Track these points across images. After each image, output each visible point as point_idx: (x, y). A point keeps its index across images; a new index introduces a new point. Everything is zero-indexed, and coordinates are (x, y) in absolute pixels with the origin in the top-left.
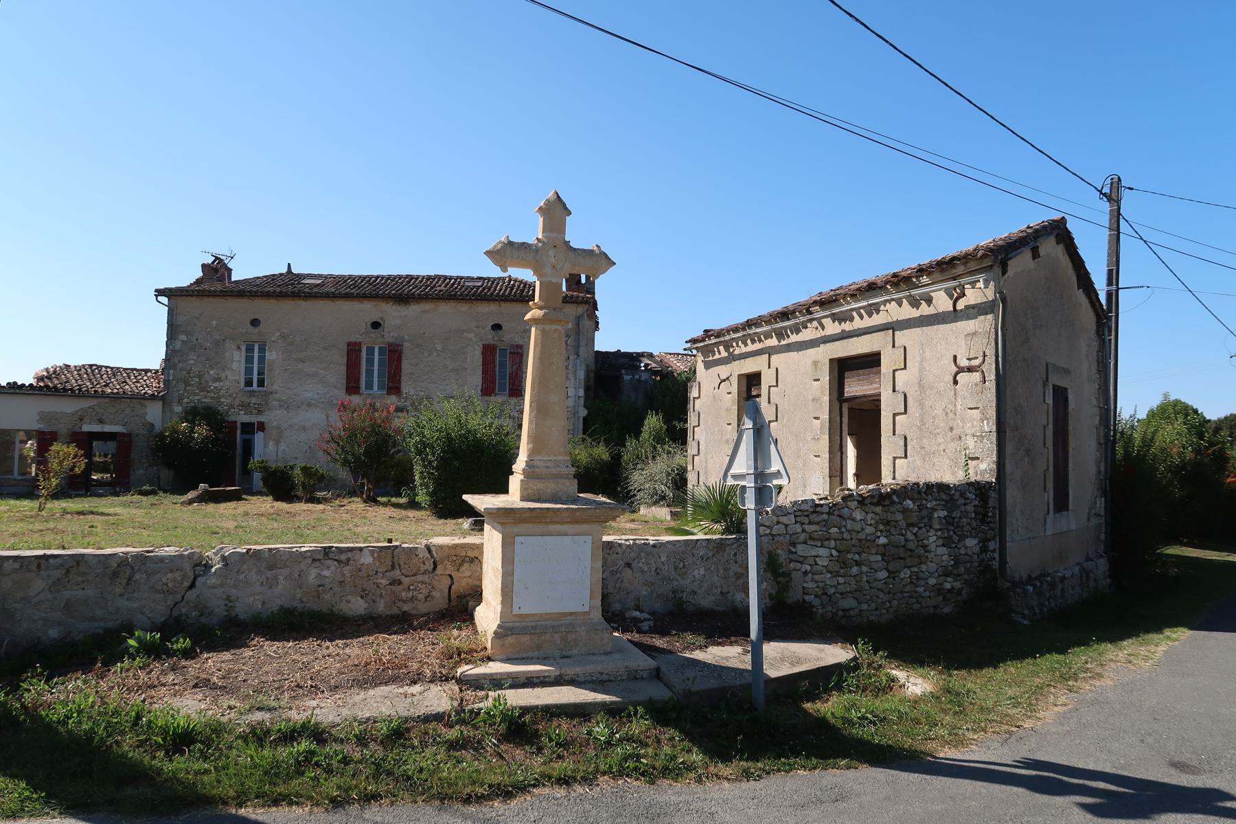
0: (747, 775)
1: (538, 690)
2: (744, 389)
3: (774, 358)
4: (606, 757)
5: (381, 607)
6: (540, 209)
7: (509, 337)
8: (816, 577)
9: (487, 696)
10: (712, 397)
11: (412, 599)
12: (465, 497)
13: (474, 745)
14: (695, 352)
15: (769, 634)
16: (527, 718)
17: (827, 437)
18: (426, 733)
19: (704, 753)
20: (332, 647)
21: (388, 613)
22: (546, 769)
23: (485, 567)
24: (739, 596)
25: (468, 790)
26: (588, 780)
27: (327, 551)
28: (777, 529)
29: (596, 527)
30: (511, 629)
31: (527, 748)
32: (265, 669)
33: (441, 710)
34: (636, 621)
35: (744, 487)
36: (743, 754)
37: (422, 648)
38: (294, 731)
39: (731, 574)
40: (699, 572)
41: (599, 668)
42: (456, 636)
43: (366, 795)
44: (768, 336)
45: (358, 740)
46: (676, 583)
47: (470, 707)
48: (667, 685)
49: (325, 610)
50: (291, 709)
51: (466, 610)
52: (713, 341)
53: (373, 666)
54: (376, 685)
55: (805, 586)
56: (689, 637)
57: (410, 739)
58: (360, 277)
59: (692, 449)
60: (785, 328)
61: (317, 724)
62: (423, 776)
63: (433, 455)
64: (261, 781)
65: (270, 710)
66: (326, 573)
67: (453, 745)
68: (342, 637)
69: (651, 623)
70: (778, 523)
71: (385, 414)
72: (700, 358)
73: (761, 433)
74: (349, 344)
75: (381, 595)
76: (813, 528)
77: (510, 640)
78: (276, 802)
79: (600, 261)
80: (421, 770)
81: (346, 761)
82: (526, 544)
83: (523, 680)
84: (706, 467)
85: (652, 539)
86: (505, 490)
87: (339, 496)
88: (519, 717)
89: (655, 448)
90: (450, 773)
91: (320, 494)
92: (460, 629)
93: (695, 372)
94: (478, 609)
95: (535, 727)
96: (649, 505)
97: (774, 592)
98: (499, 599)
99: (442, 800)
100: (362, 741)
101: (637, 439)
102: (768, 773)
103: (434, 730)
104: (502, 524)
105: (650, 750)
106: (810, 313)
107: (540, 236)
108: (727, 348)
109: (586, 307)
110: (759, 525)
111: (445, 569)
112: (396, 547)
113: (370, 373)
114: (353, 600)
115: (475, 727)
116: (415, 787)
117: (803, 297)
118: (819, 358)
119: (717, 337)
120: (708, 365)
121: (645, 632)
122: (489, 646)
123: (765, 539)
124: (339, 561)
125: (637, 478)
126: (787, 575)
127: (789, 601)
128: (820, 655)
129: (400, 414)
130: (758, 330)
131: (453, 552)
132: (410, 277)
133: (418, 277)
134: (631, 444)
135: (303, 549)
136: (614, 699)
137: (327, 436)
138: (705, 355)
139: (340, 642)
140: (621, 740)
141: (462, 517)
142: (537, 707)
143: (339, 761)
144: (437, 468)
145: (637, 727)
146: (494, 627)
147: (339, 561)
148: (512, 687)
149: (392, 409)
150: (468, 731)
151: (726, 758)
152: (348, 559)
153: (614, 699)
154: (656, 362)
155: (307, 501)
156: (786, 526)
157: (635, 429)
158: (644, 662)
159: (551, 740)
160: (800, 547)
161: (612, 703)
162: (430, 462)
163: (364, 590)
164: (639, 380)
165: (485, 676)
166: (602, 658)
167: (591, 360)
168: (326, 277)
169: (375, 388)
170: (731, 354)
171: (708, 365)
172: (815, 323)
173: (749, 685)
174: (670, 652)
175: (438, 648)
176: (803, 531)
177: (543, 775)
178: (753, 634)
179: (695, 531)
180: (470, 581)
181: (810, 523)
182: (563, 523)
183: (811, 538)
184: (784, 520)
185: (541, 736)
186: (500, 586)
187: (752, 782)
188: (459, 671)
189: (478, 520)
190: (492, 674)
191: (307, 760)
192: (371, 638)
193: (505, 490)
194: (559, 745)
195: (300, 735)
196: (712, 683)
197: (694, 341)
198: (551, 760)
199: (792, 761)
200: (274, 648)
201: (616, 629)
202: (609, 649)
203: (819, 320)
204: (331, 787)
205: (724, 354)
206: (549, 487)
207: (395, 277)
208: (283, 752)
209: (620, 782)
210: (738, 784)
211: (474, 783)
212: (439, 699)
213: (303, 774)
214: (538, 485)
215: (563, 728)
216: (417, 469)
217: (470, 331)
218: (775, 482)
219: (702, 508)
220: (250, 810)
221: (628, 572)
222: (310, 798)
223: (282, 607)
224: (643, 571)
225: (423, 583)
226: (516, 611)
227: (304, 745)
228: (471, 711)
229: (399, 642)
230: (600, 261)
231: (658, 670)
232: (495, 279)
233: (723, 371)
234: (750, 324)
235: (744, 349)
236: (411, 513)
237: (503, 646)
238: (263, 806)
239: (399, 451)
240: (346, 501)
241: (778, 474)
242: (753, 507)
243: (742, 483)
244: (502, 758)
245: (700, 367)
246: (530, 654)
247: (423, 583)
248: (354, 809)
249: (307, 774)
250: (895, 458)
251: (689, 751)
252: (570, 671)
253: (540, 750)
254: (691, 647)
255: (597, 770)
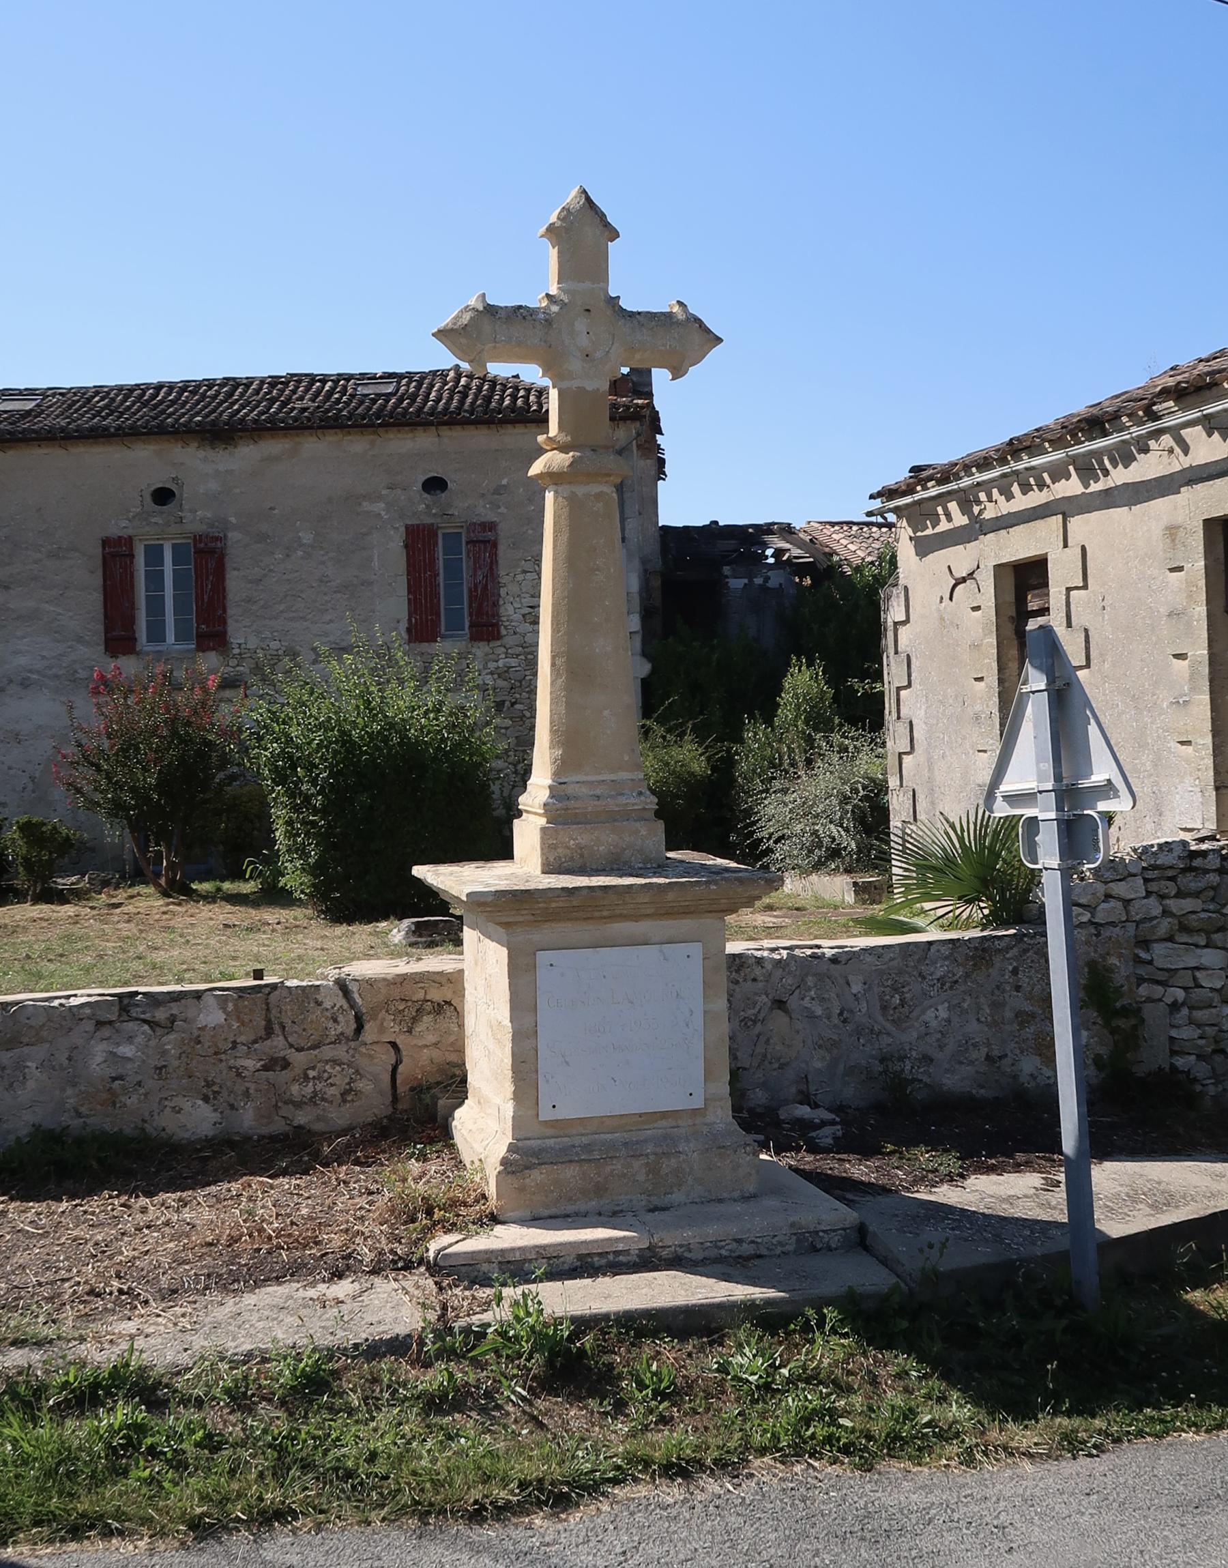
0: (1072, 1445)
1: (604, 1282)
2: (1010, 597)
3: (1075, 523)
4: (763, 1416)
5: (248, 1119)
6: (551, 230)
7: (467, 504)
8: (1198, 1015)
9: (499, 1299)
10: (937, 621)
11: (314, 1099)
12: (418, 871)
13: (486, 1404)
14: (891, 517)
15: (1105, 1141)
16: (588, 1341)
17: (1206, 698)
18: (375, 1380)
19: (976, 1404)
20: (158, 1208)
21: (265, 1131)
22: (639, 1446)
23: (470, 1022)
24: (1029, 1065)
25: (476, 1494)
26: (729, 1466)
27: (125, 1002)
28: (1107, 910)
29: (709, 922)
30: (537, 1153)
31: (593, 1403)
32: (20, 1258)
33: (401, 1330)
34: (805, 1126)
35: (1033, 821)
36: (1060, 1402)
37: (348, 1201)
38: (96, 1385)
39: (1008, 1014)
40: (937, 1014)
41: (734, 1230)
42: (418, 1175)
43: (262, 1512)
44: (1058, 473)
45: (233, 1398)
46: (886, 1040)
47: (461, 1323)
48: (884, 1262)
49: (128, 1130)
50: (82, 1339)
51: (432, 1118)
52: (933, 492)
53: (245, 1243)
54: (258, 1284)
55: (1172, 1038)
56: (924, 1157)
57: (341, 1394)
58: (120, 388)
59: (895, 739)
60: (1098, 454)
61: (142, 1369)
62: (380, 1468)
63: (314, 782)
64: (42, 1490)
65: (39, 1344)
66: (126, 1050)
67: (435, 1404)
68: (171, 1187)
69: (838, 1130)
70: (1108, 896)
71: (198, 695)
72: (905, 531)
73: (1065, 701)
74: (106, 542)
75: (247, 1093)
76: (1188, 904)
77: (537, 1176)
78: (76, 1532)
79: (684, 338)
80: (373, 1457)
81: (212, 1443)
82: (556, 968)
83: (570, 1260)
84: (931, 780)
85: (828, 946)
86: (504, 851)
87: (106, 883)
88: (570, 1339)
89: (810, 740)
90: (434, 1461)
91: (64, 882)
92: (423, 1158)
93: (893, 562)
94: (458, 1113)
95: (606, 1358)
96: (805, 872)
97: (1103, 1051)
98: (509, 1088)
99: (423, 1516)
100: (240, 1400)
101: (769, 722)
102: (1117, 1441)
103: (392, 1372)
104: (506, 925)
105: (858, 1400)
106: (1155, 417)
107: (553, 291)
108: (965, 507)
109: (633, 428)
110: (1070, 903)
111: (382, 1030)
112: (274, 987)
113: (155, 605)
114: (187, 1105)
115: (477, 1364)
116: (361, 1490)
117: (1134, 375)
118: (1180, 518)
119: (940, 482)
120: (924, 548)
121: (826, 1150)
122: (492, 1190)
123: (1082, 935)
124: (153, 1024)
125: (774, 812)
126: (1133, 1011)
127: (1140, 1071)
128: (1216, 1186)
129: (227, 693)
130: (1037, 461)
131: (396, 993)
132: (232, 383)
133: (249, 381)
134: (754, 734)
135: (74, 1002)
136: (771, 1293)
137: (70, 750)
138: (916, 525)
139: (171, 1197)
140: (791, 1381)
141: (386, 917)
142: (606, 1317)
143: (197, 1445)
144: (323, 812)
145: (826, 1352)
146: (502, 1150)
147: (153, 1024)
148: (551, 1276)
149: (213, 682)
150: (464, 1374)
151: (1023, 1412)
152: (173, 1019)
153: (771, 1293)
154: (800, 544)
155: (37, 899)
156: (1127, 902)
157: (764, 703)
158: (831, 1214)
159: (641, 1386)
160: (1159, 949)
161: (769, 1302)
162: (307, 798)
163: (209, 1084)
164: (763, 588)
165: (488, 1256)
166: (738, 1207)
167: (653, 547)
168: (44, 393)
169: (170, 637)
170: (975, 519)
171: (924, 548)
172: (1167, 440)
173: (1064, 1257)
174: (885, 1190)
175: (381, 1201)
176: (1166, 913)
177: (632, 1459)
178: (1069, 1139)
179: (919, 921)
180: (436, 1054)
181: (1180, 894)
182: (636, 918)
183: (1184, 928)
184: (1120, 889)
185: (620, 1377)
186: (508, 1061)
187: (1083, 1461)
188: (433, 1246)
189: (437, 921)
190: (503, 1252)
191: (131, 1445)
192: (235, 1186)
193: (504, 851)
194: (660, 1395)
195: (109, 1394)
196: (983, 1254)
197: (888, 493)
198: (646, 1428)
199: (1168, 1412)
200: (30, 1215)
201: (764, 1146)
202: (751, 1188)
203: (1175, 431)
204: (187, 1496)
205: (960, 520)
206: (603, 840)
207: (199, 384)
208: (77, 1430)
209: (798, 1468)
210: (1052, 1465)
211: (486, 1479)
212: (394, 1307)
213: (125, 1473)
214: (578, 837)
215: (665, 1358)
216: (279, 814)
217: (380, 498)
218: (1103, 806)
219: (936, 873)
220: (25, 1549)
221: (780, 1018)
222: (147, 1521)
223: (37, 1127)
224: (812, 1017)
225: (335, 1062)
226: (546, 1114)
227: (122, 1413)
228: (467, 1331)
229: (296, 1192)
230: (684, 338)
231: (862, 1229)
232: (423, 376)
233: (960, 558)
234: (1015, 448)
235: (1006, 507)
236: (271, 915)
237: (522, 1189)
238: (51, 1541)
239: (233, 778)
240: (121, 895)
241: (1108, 789)
242: (1055, 862)
243: (1029, 812)
244: (541, 1426)
245: (906, 552)
246: (582, 1206)
247: (335, 1062)
248: (240, 1542)
249: (134, 1473)
250: (1069, 590)
251: (942, 1399)
252: (672, 1239)
253: (620, 1407)
254: (931, 1178)
255: (746, 1446)
